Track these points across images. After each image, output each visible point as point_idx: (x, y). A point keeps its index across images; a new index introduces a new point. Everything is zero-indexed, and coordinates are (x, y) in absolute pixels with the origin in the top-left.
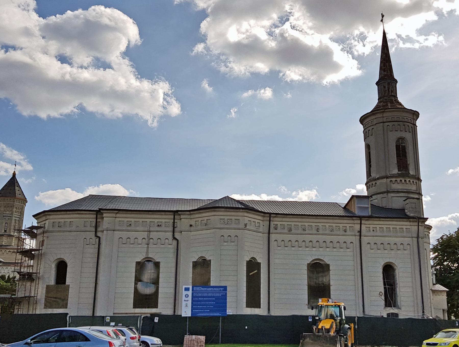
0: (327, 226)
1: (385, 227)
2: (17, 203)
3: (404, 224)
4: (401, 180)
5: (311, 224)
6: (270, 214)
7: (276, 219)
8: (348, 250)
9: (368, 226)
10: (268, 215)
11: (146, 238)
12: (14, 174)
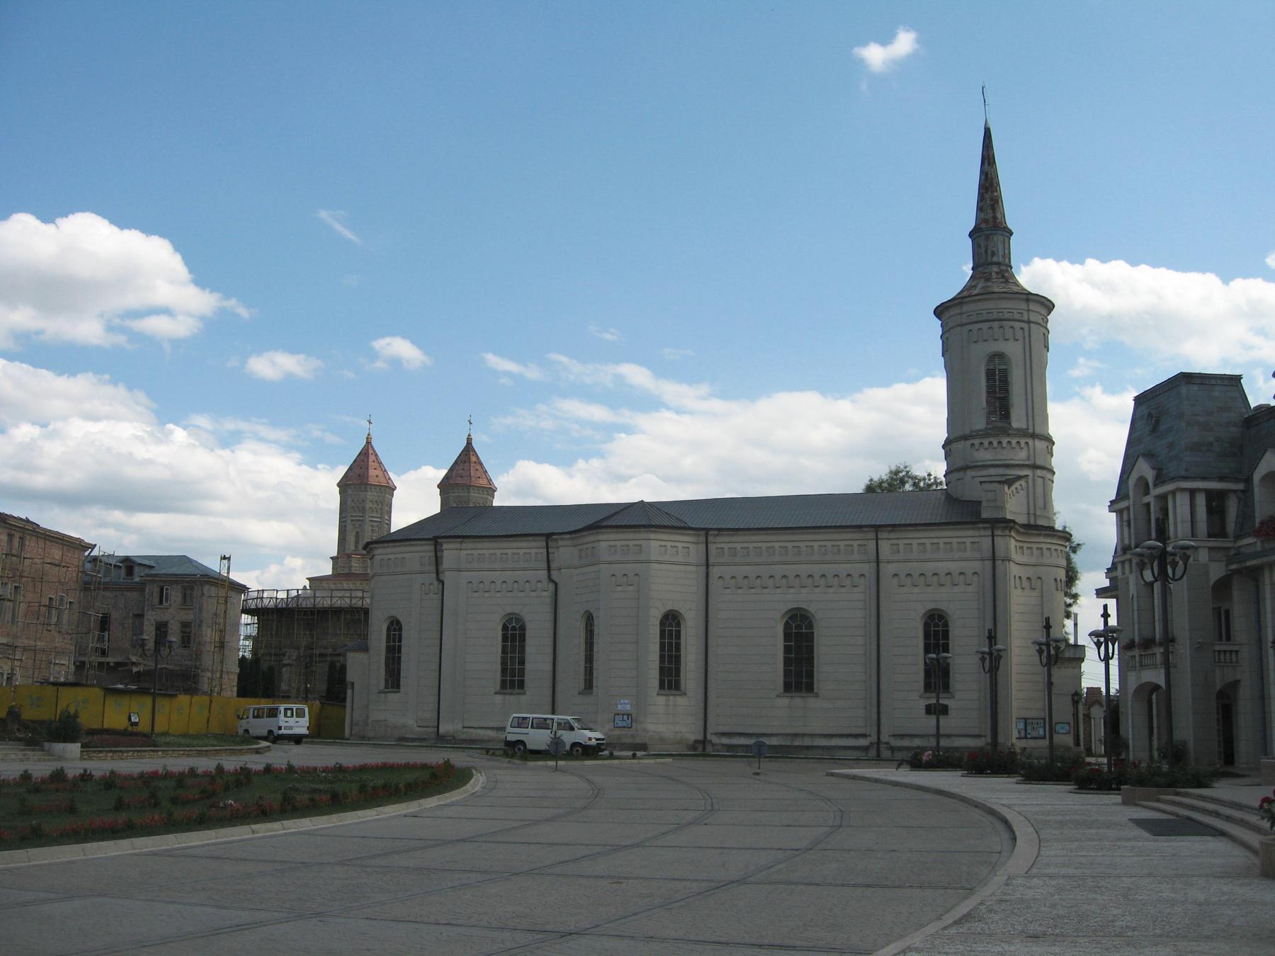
0: (842, 547)
1: (790, 545)
2: (370, 495)
3: (967, 536)
4: (991, 443)
5: (745, 545)
6: (707, 530)
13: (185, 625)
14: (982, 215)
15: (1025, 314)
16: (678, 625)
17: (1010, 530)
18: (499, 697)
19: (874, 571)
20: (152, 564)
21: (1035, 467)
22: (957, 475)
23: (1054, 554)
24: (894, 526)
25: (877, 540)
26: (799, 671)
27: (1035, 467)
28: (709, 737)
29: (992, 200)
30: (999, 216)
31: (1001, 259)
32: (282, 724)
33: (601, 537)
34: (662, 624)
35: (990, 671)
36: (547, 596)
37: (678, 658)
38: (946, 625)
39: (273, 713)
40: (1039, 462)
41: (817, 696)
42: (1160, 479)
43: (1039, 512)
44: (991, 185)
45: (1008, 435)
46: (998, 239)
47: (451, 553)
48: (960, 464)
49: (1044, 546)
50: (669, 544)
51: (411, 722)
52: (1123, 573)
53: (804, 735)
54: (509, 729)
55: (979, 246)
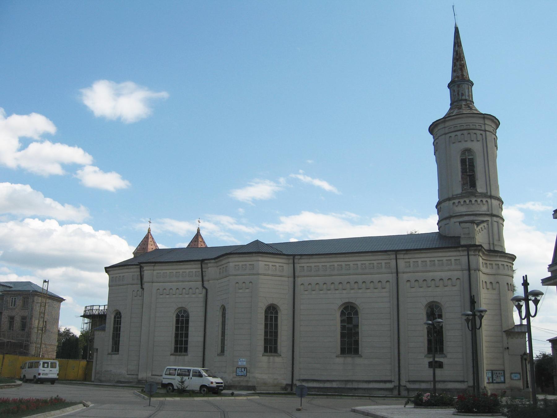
0: (375, 264)
1: (343, 264)
3: (452, 256)
4: (465, 201)
6: (294, 256)
8: (384, 290)
9: (408, 260)
10: (292, 257)
11: (391, 281)
12: (149, 232)
13: (24, 318)
14: (455, 74)
15: (483, 126)
16: (277, 313)
17: (479, 251)
19: (395, 279)
20: (11, 286)
21: (492, 215)
22: (444, 222)
23: (506, 267)
24: (407, 250)
25: (396, 259)
26: (350, 344)
27: (492, 215)
28: (295, 382)
29: (461, 65)
30: (465, 74)
31: (467, 98)
32: (41, 372)
33: (230, 260)
34: (266, 312)
35: (472, 329)
36: (202, 296)
37: (276, 333)
39: (37, 365)
40: (495, 212)
41: (361, 356)
43: (495, 243)
44: (460, 57)
45: (475, 196)
46: (465, 86)
47: (148, 272)
48: (447, 215)
49: (500, 263)
50: (271, 264)
51: (124, 372)
53: (352, 381)
54: (164, 376)
55: (454, 91)
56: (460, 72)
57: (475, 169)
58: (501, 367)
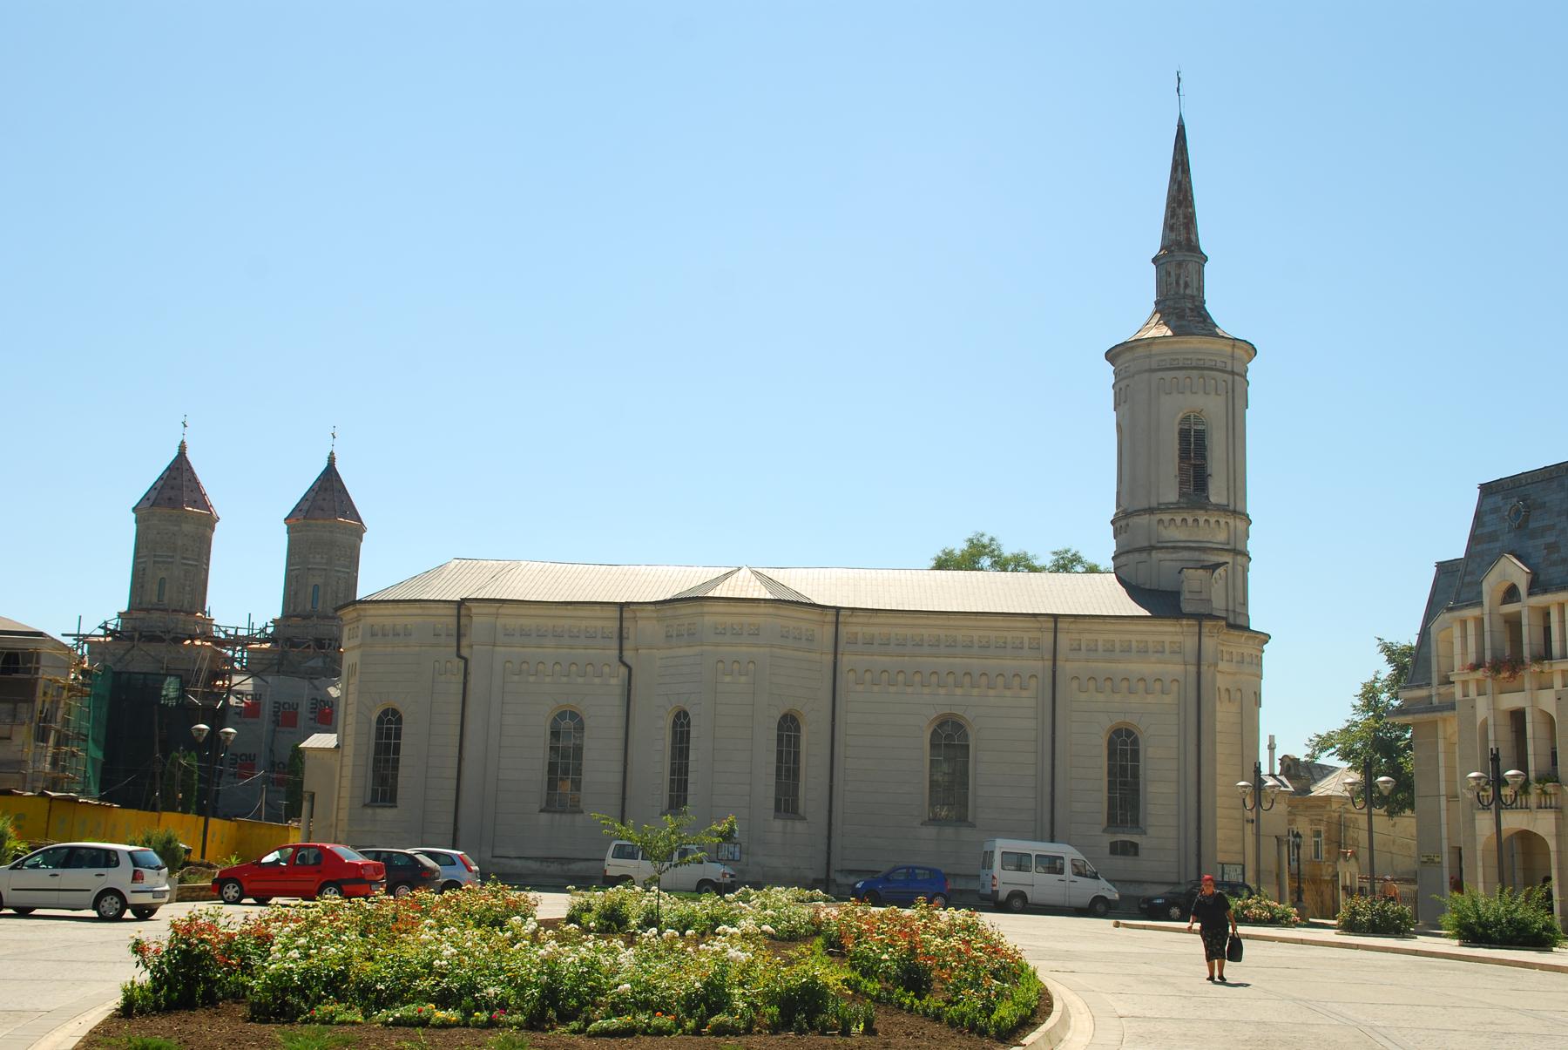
2: (187, 528)
4: (1184, 520)
7: (854, 620)
8: (1024, 693)
14: (1173, 236)
18: (544, 816)
28: (833, 875)
36: (616, 681)
38: (1135, 742)
41: (972, 826)
42: (1536, 586)
52: (1465, 695)
54: (609, 860)
55: (1168, 274)
56: (1183, 231)
57: (1208, 454)
58: (1239, 859)
